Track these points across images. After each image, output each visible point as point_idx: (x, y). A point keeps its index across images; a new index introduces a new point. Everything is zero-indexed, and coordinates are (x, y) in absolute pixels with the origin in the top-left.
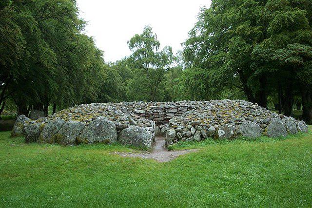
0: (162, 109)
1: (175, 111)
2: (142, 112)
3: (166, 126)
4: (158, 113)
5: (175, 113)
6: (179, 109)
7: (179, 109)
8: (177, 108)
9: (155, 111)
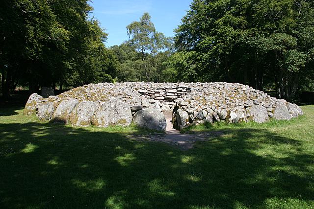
0: (163, 89)
1: (175, 91)
2: (145, 91)
4: (159, 92)
7: (179, 89)
8: (177, 89)
9: (157, 91)
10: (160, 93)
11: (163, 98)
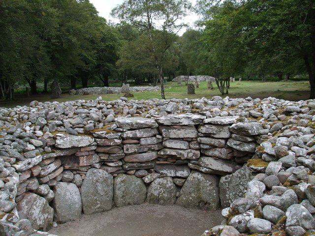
1: (191, 133)
3: (163, 176)
4: (139, 139)
5: (189, 141)
6: (203, 129)
8: (197, 127)
10: (143, 142)
11: (153, 155)
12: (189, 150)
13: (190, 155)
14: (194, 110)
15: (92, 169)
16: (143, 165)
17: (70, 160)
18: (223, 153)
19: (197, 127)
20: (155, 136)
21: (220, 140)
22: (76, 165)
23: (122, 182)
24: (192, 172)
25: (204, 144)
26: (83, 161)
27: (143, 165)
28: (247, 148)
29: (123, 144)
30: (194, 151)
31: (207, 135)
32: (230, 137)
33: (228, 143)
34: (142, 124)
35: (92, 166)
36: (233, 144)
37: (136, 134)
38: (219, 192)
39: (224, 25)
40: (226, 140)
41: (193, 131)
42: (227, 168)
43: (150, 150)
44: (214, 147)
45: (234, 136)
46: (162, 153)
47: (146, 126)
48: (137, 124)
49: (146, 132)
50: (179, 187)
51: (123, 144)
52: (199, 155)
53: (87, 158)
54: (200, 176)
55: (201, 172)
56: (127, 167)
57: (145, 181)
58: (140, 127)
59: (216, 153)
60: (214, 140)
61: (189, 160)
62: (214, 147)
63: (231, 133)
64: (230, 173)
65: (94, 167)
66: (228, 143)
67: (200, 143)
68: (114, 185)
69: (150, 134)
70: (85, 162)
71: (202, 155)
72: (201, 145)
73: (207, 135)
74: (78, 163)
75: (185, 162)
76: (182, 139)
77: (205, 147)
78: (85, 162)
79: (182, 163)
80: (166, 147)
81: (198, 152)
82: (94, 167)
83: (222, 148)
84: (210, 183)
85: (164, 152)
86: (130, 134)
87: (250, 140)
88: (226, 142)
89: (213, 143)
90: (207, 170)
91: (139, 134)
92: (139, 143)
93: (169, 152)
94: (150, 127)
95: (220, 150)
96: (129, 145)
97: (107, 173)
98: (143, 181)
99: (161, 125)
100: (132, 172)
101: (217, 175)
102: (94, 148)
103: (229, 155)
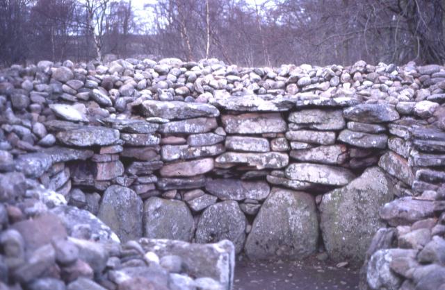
4: (186, 136)
8: (285, 116)
12: (270, 154)
13: (273, 162)
14: (312, 32)
15: (113, 187)
16: (191, 181)
17: (81, 169)
18: (334, 154)
19: (285, 116)
20: (212, 130)
21: (327, 133)
22: (90, 178)
23: (157, 210)
24: (274, 189)
25: (297, 141)
26: (103, 173)
27: (191, 181)
28: (375, 142)
29: (162, 145)
30: (277, 154)
31: (306, 127)
32: (345, 127)
33: (341, 138)
34: (194, 111)
35: (112, 182)
36: (349, 137)
37: (184, 128)
38: (319, 221)
39: (273, 79)
40: (337, 132)
41: (278, 121)
42: (335, 178)
43: (205, 155)
44: (314, 144)
45: (351, 125)
46: (223, 159)
47: (200, 114)
48: (186, 109)
49: (200, 123)
50: (250, 218)
51: (162, 145)
52: (287, 161)
53: (108, 165)
54: (289, 197)
55: (291, 189)
56: (164, 185)
57: (193, 207)
58: (191, 116)
59: (317, 154)
60: (316, 133)
61: (269, 170)
62: (314, 144)
63: (347, 120)
64: (340, 187)
65: (117, 183)
66: (341, 138)
67: (289, 141)
68: (144, 216)
69: (206, 129)
70: (105, 173)
71: (293, 160)
72: (292, 144)
73: (306, 127)
74: (95, 175)
75: (263, 173)
76: (259, 135)
77: (299, 146)
78: (105, 173)
79: (260, 178)
80: (232, 150)
81: (286, 156)
82: (117, 183)
83: (329, 145)
84: (305, 205)
85: (227, 157)
86: (175, 127)
87: (379, 128)
88: (337, 135)
89: (314, 139)
90: (302, 184)
91: (188, 127)
92: (185, 143)
93: (235, 157)
94: (206, 115)
95: (326, 149)
96: (170, 147)
97: (136, 195)
98: (188, 206)
99: (224, 111)
100: (173, 194)
101: (316, 190)
102: (119, 149)
103: (341, 157)
